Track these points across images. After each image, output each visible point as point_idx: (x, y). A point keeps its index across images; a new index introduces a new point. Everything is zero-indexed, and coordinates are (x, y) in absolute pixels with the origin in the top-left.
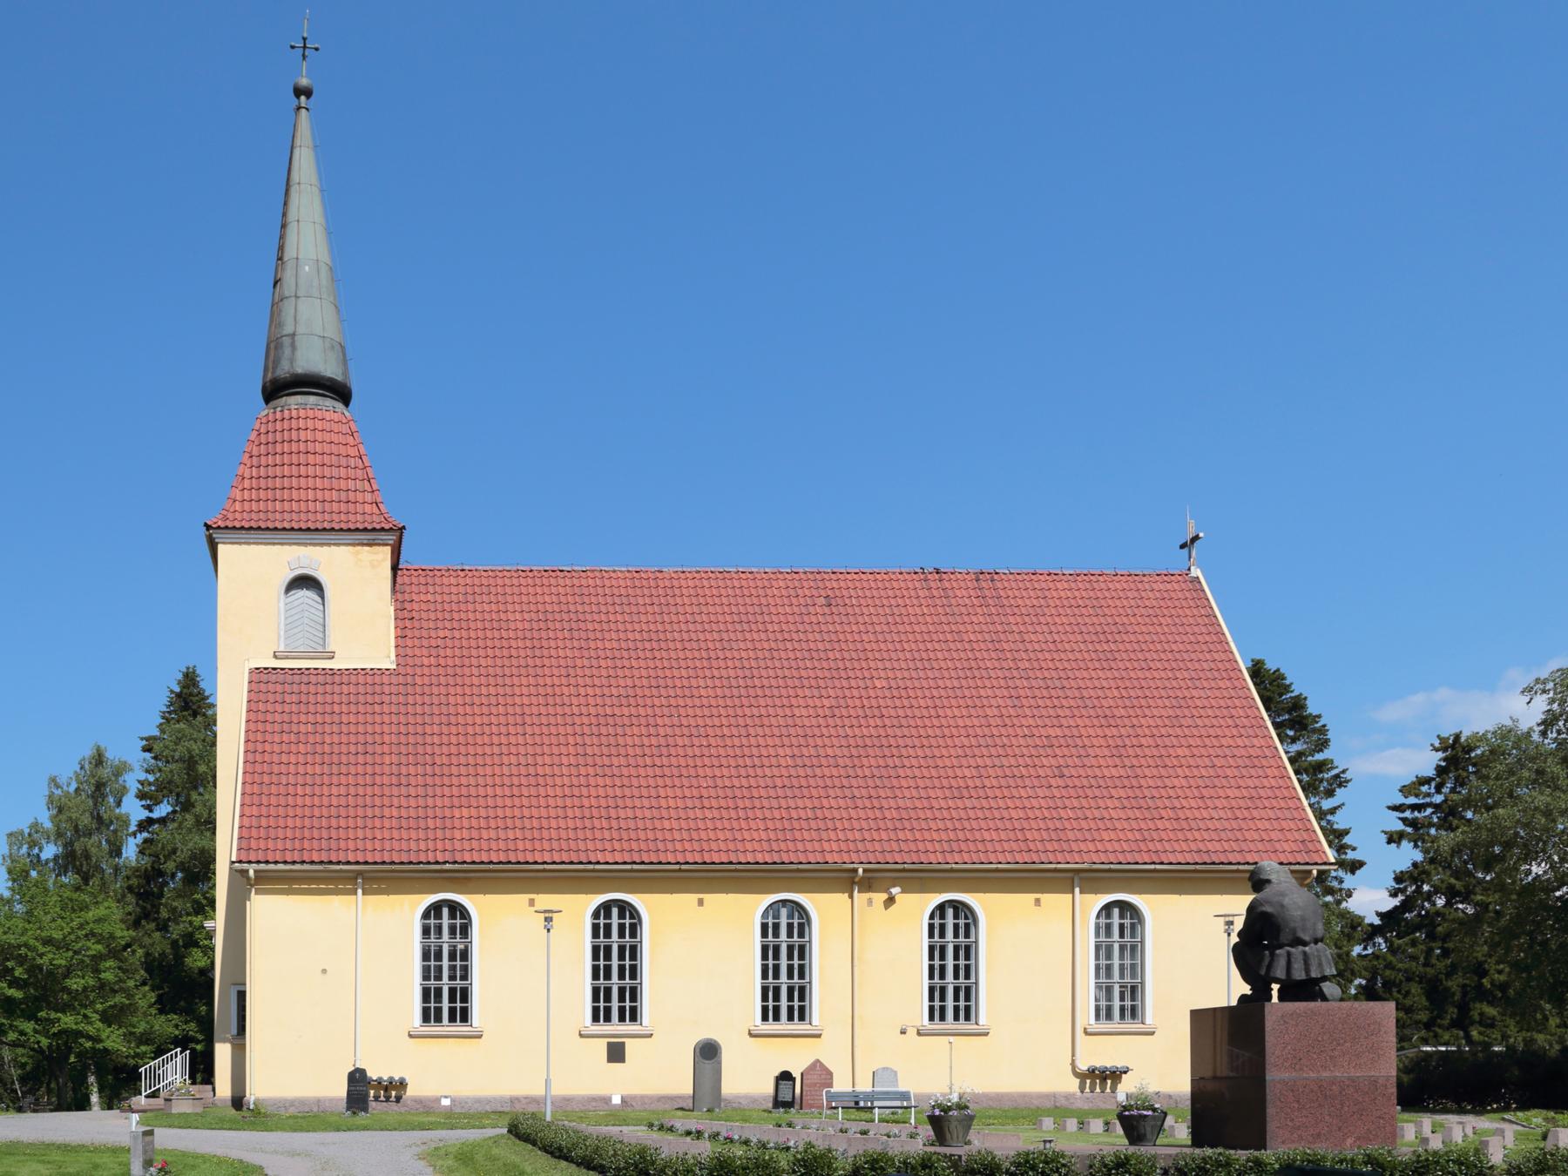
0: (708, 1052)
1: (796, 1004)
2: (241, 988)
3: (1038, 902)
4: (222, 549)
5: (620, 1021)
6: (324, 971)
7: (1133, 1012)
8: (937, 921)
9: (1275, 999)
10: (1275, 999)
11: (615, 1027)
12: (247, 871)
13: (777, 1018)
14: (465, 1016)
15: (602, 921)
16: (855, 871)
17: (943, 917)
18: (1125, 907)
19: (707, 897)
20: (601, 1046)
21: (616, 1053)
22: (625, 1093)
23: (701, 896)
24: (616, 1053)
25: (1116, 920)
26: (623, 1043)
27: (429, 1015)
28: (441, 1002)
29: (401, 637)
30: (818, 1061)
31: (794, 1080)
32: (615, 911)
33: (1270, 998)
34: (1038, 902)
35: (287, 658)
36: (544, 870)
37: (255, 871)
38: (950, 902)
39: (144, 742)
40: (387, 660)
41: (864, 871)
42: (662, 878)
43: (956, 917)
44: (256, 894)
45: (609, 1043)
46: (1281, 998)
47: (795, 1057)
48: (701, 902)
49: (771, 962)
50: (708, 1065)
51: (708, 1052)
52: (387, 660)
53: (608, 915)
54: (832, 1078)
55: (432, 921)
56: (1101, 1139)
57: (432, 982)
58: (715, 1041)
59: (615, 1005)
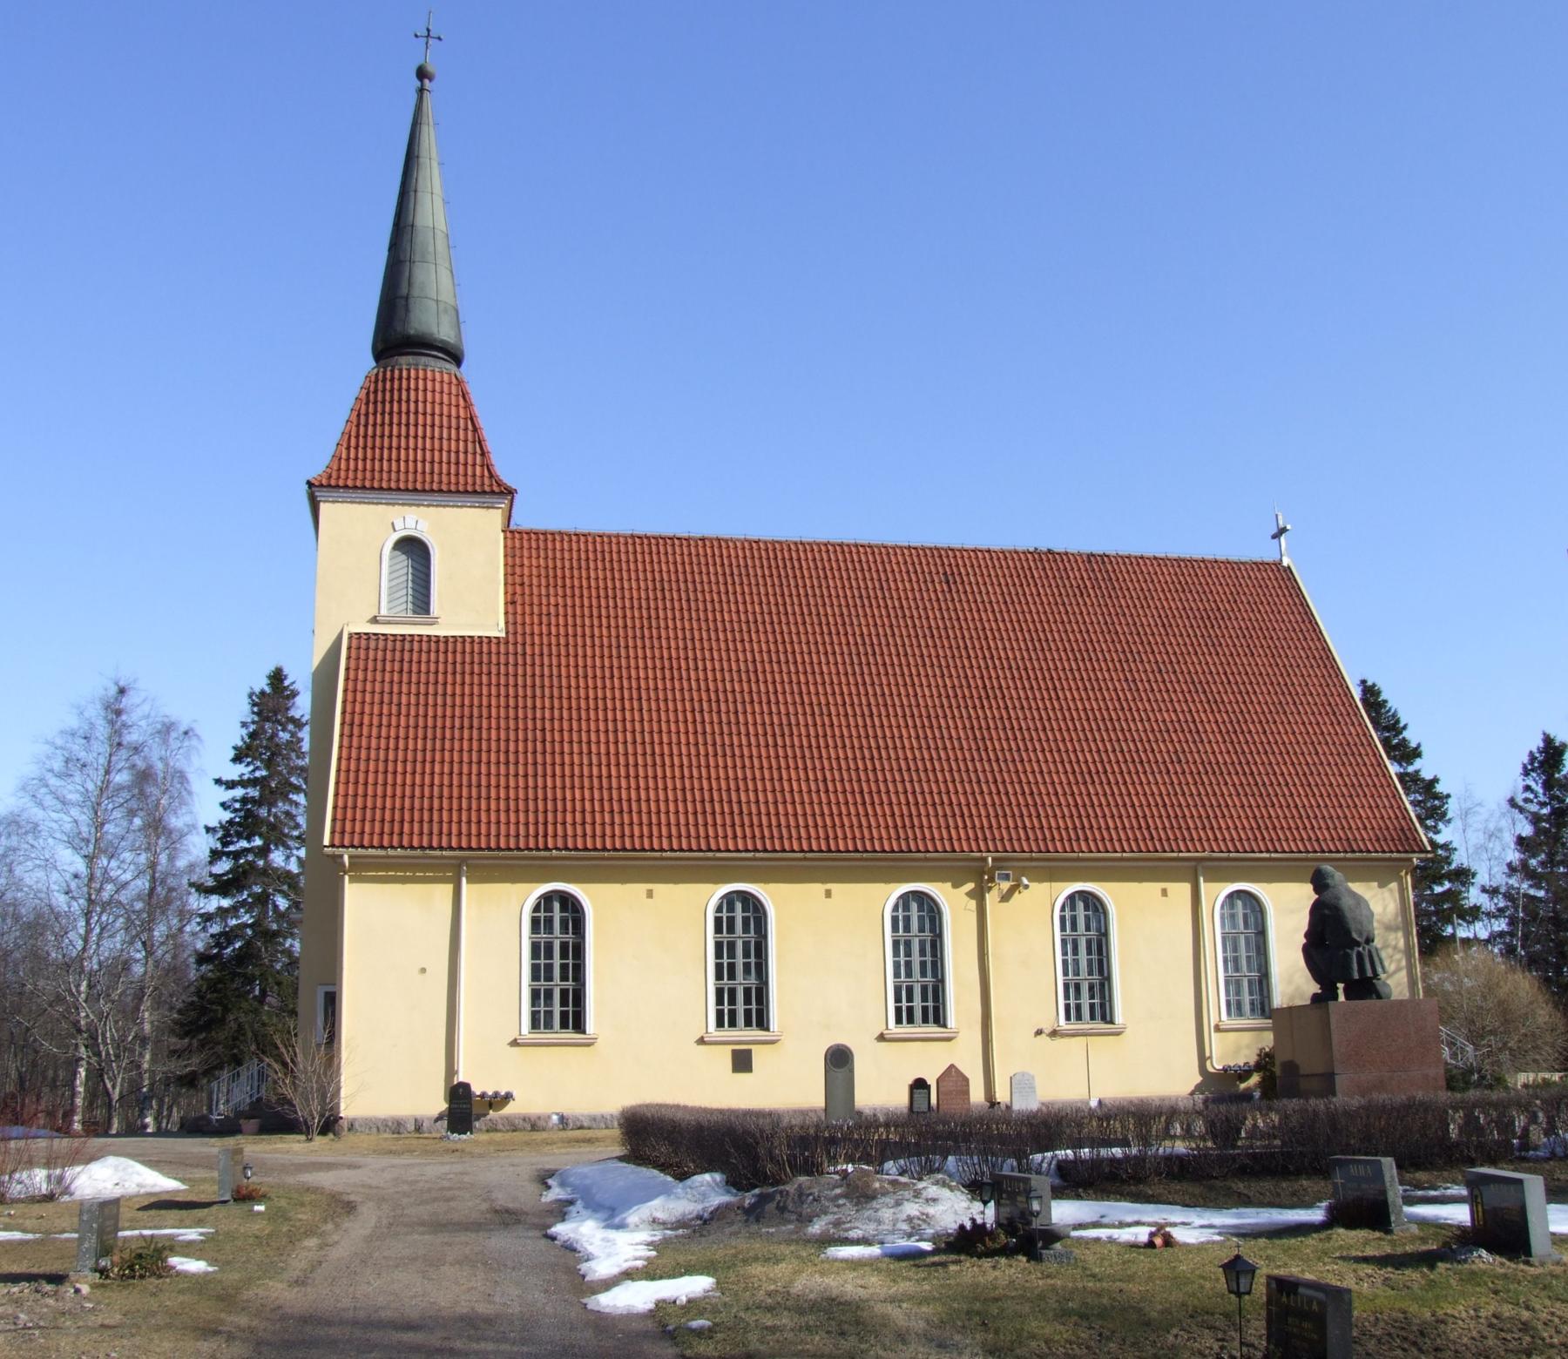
0: (839, 1060)
1: (904, 1004)
2: (330, 989)
3: (650, 894)
4: (324, 508)
5: (562, 1027)
6: (423, 970)
7: (575, 1020)
8: (724, 915)
9: (1342, 998)
10: (1342, 998)
11: (744, 1034)
12: (341, 856)
13: (733, 1024)
14: (579, 1026)
15: (542, 915)
16: (985, 860)
17: (1073, 908)
18: (920, 897)
19: (835, 887)
20: (724, 1056)
21: (742, 1062)
22: (1102, 1096)
23: (829, 886)
24: (742, 1062)
25: (739, 914)
26: (749, 1051)
27: (904, 1015)
28: (551, 1005)
29: (511, 602)
30: (952, 1066)
31: (928, 1087)
32: (739, 906)
33: (1336, 998)
34: (1164, 892)
35: (389, 623)
36: (603, 858)
37: (351, 857)
38: (1081, 893)
39: (1402, 725)
40: (494, 626)
41: (993, 859)
42: (1087, 868)
43: (920, 909)
44: (350, 882)
45: (734, 1052)
46: (1347, 998)
47: (929, 1062)
48: (828, 894)
49: (725, 961)
50: (840, 1074)
51: (839, 1060)
52: (494, 626)
53: (549, 909)
54: (968, 1085)
55: (542, 915)
56: (433, 1169)
57: (543, 983)
58: (838, 1045)
59: (740, 1008)
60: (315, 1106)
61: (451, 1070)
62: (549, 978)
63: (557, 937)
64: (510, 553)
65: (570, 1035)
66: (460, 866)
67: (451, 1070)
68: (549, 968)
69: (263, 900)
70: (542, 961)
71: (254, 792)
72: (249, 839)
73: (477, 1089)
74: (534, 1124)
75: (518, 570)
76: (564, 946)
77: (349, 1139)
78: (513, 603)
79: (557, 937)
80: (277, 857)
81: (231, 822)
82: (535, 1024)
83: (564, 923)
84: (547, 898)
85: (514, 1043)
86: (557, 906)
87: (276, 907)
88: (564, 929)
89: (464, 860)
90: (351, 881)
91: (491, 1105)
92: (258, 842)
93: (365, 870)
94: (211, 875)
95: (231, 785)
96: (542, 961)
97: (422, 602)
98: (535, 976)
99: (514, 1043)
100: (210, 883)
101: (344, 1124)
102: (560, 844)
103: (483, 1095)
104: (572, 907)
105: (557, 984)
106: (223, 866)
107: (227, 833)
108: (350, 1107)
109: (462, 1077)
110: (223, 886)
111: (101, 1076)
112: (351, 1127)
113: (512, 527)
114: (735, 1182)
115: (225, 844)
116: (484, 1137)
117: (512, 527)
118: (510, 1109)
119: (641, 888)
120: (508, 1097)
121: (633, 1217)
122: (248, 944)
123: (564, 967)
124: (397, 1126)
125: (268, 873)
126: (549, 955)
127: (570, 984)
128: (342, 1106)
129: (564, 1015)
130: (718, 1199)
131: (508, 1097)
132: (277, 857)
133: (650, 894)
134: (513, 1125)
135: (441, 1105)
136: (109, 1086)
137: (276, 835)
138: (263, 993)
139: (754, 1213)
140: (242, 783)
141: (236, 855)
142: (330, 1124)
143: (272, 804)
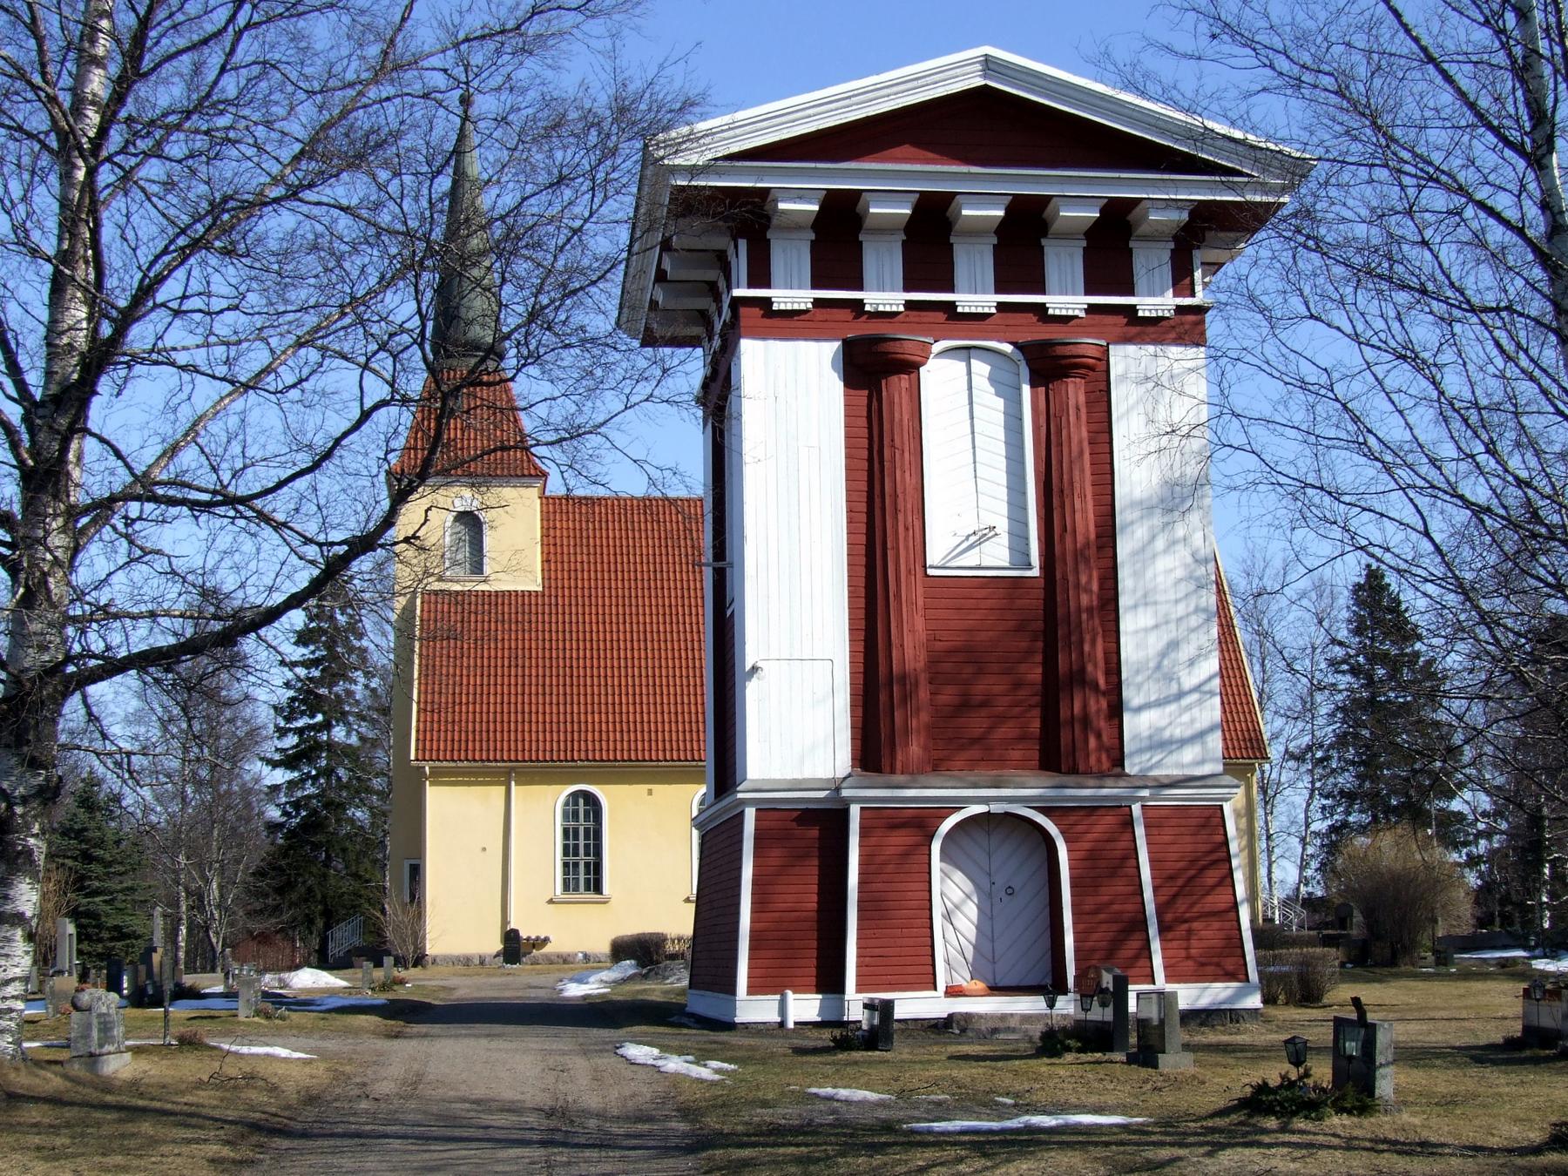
3: (650, 792)
7: (596, 885)
14: (598, 888)
29: (546, 561)
40: (532, 581)
52: (532, 581)
60: (411, 948)
61: (505, 920)
62: (576, 854)
63: (582, 824)
64: (546, 517)
65: (592, 896)
66: (509, 774)
67: (505, 920)
68: (576, 847)
69: (328, 772)
70: (571, 842)
71: (316, 673)
72: (312, 716)
73: (524, 934)
74: (565, 959)
75: (552, 532)
76: (587, 831)
77: (431, 970)
78: (548, 561)
79: (582, 824)
80: (339, 733)
81: (293, 699)
82: (566, 888)
83: (587, 814)
84: (575, 795)
85: (551, 902)
86: (581, 801)
87: (339, 779)
88: (587, 818)
89: (513, 768)
90: (432, 784)
91: (534, 946)
92: (319, 718)
93: (439, 777)
94: (277, 750)
95: (293, 665)
96: (571, 842)
97: (477, 567)
98: (566, 852)
99: (551, 902)
100: (277, 757)
101: (429, 959)
102: (583, 756)
103: (528, 939)
104: (592, 802)
105: (582, 859)
106: (291, 740)
107: (288, 712)
108: (432, 948)
109: (513, 925)
110: (289, 762)
111: (207, 931)
112: (434, 962)
113: (547, 493)
114: (641, 964)
115: (288, 719)
116: (529, 967)
117: (547, 493)
118: (548, 949)
119: (645, 787)
120: (546, 940)
121: (592, 979)
122: (313, 813)
123: (587, 846)
124: (466, 961)
125: (330, 746)
126: (576, 837)
127: (591, 858)
128: (428, 946)
129: (587, 881)
130: (631, 972)
131: (546, 940)
132: (339, 733)
133: (650, 792)
134: (550, 960)
135: (499, 947)
136: (214, 940)
137: (336, 712)
138: (328, 857)
139: (645, 977)
140: (307, 664)
141: (300, 731)
142: (420, 960)
143: (330, 686)
